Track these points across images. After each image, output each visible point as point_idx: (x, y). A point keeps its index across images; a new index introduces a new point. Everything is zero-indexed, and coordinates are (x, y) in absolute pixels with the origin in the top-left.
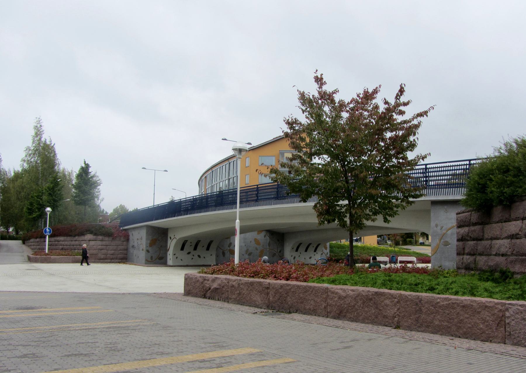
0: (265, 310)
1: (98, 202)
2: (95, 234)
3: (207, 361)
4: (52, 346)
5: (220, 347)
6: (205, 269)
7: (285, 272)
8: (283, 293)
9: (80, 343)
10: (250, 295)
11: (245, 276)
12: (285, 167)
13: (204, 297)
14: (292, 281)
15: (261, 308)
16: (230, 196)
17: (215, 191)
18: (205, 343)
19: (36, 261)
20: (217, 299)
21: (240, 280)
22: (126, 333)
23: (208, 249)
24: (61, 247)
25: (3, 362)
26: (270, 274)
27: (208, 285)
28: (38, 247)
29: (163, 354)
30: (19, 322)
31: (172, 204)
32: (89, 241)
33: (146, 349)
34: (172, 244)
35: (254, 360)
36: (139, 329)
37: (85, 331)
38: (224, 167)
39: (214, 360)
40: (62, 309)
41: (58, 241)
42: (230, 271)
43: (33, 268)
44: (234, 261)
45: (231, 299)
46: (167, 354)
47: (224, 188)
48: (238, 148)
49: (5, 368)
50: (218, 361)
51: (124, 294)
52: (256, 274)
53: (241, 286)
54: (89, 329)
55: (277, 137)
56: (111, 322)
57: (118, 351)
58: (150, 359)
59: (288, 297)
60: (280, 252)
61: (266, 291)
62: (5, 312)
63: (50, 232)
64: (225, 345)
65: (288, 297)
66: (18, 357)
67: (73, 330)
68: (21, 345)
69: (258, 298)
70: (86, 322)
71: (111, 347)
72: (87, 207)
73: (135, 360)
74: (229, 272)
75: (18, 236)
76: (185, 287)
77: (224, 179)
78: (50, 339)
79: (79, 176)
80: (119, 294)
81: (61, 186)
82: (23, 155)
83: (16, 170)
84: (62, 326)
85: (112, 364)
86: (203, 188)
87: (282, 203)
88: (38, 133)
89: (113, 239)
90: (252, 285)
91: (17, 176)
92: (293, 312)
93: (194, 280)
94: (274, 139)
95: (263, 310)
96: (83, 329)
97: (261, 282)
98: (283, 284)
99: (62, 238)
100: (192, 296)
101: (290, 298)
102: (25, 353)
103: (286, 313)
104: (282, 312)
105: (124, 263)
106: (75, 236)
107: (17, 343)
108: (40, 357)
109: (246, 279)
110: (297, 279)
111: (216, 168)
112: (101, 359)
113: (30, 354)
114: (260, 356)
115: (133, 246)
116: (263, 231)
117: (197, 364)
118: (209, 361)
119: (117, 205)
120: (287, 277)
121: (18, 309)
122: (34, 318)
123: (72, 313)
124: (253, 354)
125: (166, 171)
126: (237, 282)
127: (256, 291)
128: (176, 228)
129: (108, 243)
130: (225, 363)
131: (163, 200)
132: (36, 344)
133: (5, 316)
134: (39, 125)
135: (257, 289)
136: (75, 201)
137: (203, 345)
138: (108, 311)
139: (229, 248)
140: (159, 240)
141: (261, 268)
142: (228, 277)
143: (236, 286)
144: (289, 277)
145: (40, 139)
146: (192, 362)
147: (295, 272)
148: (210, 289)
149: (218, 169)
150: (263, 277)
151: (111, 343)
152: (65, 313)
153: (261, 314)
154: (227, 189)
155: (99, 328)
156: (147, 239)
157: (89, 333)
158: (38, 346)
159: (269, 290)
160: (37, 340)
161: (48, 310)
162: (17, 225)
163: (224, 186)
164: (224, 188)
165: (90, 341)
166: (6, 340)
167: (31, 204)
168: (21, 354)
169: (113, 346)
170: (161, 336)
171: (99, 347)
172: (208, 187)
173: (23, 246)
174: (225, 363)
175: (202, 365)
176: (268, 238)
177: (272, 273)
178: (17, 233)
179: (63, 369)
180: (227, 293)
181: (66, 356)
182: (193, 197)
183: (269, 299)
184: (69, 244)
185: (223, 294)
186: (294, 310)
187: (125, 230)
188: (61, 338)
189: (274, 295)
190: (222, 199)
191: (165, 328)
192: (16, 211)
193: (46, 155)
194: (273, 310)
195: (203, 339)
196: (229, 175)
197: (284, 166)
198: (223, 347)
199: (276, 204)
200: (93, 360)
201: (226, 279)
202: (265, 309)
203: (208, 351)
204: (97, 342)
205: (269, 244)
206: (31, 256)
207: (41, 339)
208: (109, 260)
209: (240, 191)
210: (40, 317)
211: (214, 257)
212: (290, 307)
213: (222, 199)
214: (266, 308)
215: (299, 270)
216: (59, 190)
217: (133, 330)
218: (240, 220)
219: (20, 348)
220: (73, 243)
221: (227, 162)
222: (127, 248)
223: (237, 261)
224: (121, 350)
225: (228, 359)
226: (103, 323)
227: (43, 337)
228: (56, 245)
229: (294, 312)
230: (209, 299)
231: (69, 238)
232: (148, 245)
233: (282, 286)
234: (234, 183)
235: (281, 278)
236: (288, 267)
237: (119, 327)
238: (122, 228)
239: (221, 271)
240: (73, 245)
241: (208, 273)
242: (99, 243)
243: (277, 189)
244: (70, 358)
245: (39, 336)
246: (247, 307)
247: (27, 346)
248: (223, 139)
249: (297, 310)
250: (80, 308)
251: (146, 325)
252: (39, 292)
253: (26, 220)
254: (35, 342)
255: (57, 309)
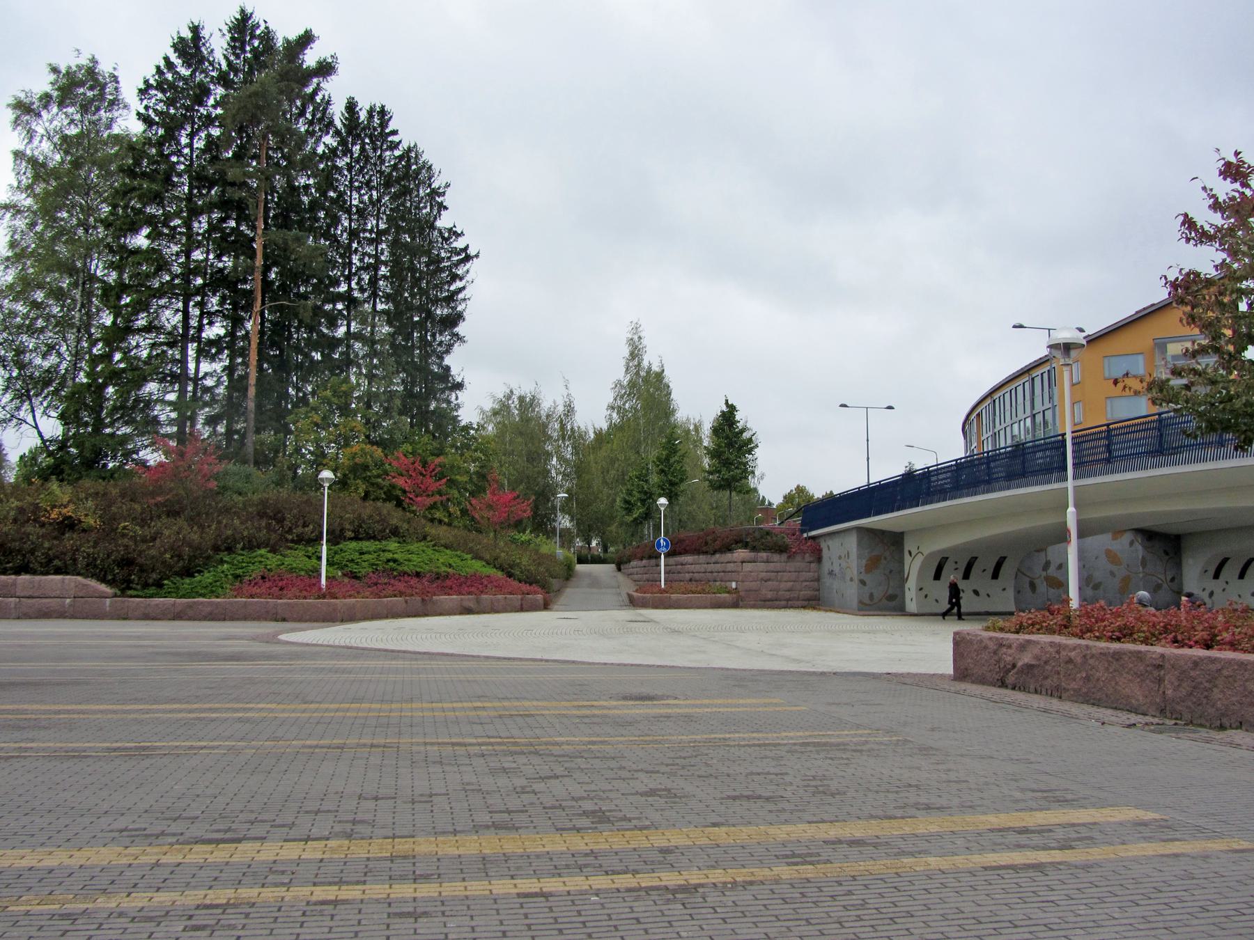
0: (1156, 720)
1: (752, 482)
2: (754, 549)
3: (1033, 832)
4: (699, 776)
5: (1059, 801)
6: (1001, 622)
7: (1200, 628)
8: (1200, 680)
9: (752, 773)
10: (1113, 683)
11: (1098, 638)
12: (1182, 377)
13: (1003, 684)
14: (1220, 650)
15: (1145, 714)
16: (1039, 455)
17: (1002, 445)
18: (1023, 790)
19: (644, 604)
20: (1032, 689)
21: (1087, 647)
22: (842, 758)
23: (995, 575)
24: (688, 576)
25: (615, 802)
26: (1161, 634)
27: (1009, 659)
28: (645, 576)
29: (929, 808)
30: (630, 724)
31: (909, 476)
32: (742, 562)
33: (891, 796)
34: (913, 567)
35: (1150, 838)
36: (869, 751)
37: (757, 748)
38: (1020, 389)
39: (1050, 831)
40: (706, 702)
41: (682, 564)
42: (1061, 625)
43: (641, 619)
44: (1067, 601)
45: (1066, 690)
46: (938, 808)
47: (1023, 437)
48: (1061, 341)
49: (620, 815)
50: (1060, 834)
51: (823, 674)
52: (1124, 634)
53: (1091, 661)
54: (765, 745)
55: (1144, 309)
56: (807, 733)
57: (833, 795)
58: (903, 818)
59: (1215, 690)
60: (1173, 580)
61: (1156, 673)
62: (605, 703)
63: (667, 546)
64: (1069, 797)
65: (1215, 690)
66: (641, 795)
67: (734, 746)
68: (642, 770)
69: (1137, 693)
70: (758, 731)
71: (816, 787)
72: (734, 494)
73: (872, 817)
74: (1057, 628)
75: (608, 555)
76: (955, 661)
77: (1021, 415)
78: (693, 761)
79: (716, 431)
80: (814, 673)
81: (682, 452)
82: (609, 397)
83: (598, 427)
84: (713, 736)
85: (823, 821)
86: (974, 438)
87: (1175, 464)
88: (635, 353)
89: (789, 557)
90: (1117, 660)
91: (599, 434)
92: (1231, 728)
93: (975, 647)
94: (1137, 312)
95: (1149, 719)
96: (754, 745)
97: (1140, 652)
98: (1200, 658)
99: (688, 558)
100: (973, 682)
101: (1222, 691)
102: (652, 786)
103: (1210, 728)
104: (1201, 725)
105: (814, 608)
106: (714, 553)
107: (634, 767)
108: (680, 797)
109: (1102, 644)
110: (1233, 646)
111: (1000, 393)
112: (800, 811)
113: (664, 790)
114: (1163, 830)
115: (831, 573)
116: (1125, 531)
117: (1012, 838)
118: (1039, 832)
119: (789, 487)
120: (1205, 640)
121: (625, 698)
122: (658, 718)
123: (726, 709)
124: (1144, 824)
125: (890, 408)
126: (1078, 651)
127: (1127, 673)
128: (924, 531)
129: (778, 566)
130: (1079, 839)
131: (887, 470)
132: (667, 769)
133: (605, 712)
134: (636, 338)
135: (1131, 669)
136: (710, 481)
137: (1018, 795)
138: (799, 708)
139: (1044, 574)
140: (885, 559)
141: (1138, 619)
142: (1057, 639)
143: (1079, 660)
144: (1212, 640)
145: (639, 364)
146: (1000, 830)
147: (1227, 629)
148: (1014, 666)
149: (1007, 396)
150: (1146, 641)
151: (814, 778)
152: (714, 710)
153: (1147, 728)
154: (1030, 438)
155: (785, 745)
156: (859, 557)
157: (768, 753)
158: (675, 774)
159: (1162, 673)
160: (670, 761)
161: (681, 702)
162: (604, 534)
163: (1022, 432)
164: (1023, 437)
165: (772, 770)
166: (613, 758)
167: (630, 493)
168: (644, 789)
169: (819, 783)
170: (919, 768)
171: (791, 784)
172: (985, 437)
173: (619, 575)
174: (1079, 839)
175: (1023, 839)
176: (1140, 548)
177: (1166, 630)
178: (605, 549)
179: (729, 825)
180: (1056, 676)
181: (729, 797)
182: (956, 460)
183: (1164, 692)
184: (703, 570)
185: (1046, 678)
186: (1233, 721)
187: (814, 538)
188: (715, 761)
189: (1176, 684)
190: (1023, 462)
191: (925, 750)
192: (602, 507)
193: (652, 395)
194: (1176, 719)
195: (1016, 780)
196: (1033, 407)
197: (1180, 374)
198: (1066, 801)
199: (1161, 465)
200: (784, 810)
201: (1052, 644)
202: (1154, 716)
203: (1031, 810)
204: (787, 774)
205: (1144, 563)
206: (635, 594)
207: (677, 761)
208: (783, 603)
209: (1073, 438)
210: (668, 717)
211: (1011, 593)
212: (1223, 715)
213: (1023, 462)
214: (1158, 715)
215: (1238, 624)
216: (679, 462)
217: (855, 751)
218: (1076, 506)
219: (641, 775)
220: (711, 567)
221: (1026, 378)
222: (819, 576)
223: (1074, 603)
224: (838, 794)
225: (1085, 832)
226: (792, 734)
227: (681, 757)
228: (679, 573)
229: (1234, 726)
230: (1014, 688)
231: (702, 558)
232: (863, 570)
233: (1196, 663)
234: (1045, 423)
235: (1192, 643)
236: (1206, 616)
237: (825, 744)
238: (805, 535)
239: (1037, 626)
240: (712, 572)
241: (1007, 629)
242: (762, 566)
243: (1159, 430)
244: (738, 802)
245: (672, 755)
246: (1109, 712)
247: (652, 772)
248: (1015, 327)
249: (1241, 723)
250: (741, 701)
251: (881, 743)
252: (658, 666)
253: (621, 524)
254: (667, 765)
255: (698, 702)
